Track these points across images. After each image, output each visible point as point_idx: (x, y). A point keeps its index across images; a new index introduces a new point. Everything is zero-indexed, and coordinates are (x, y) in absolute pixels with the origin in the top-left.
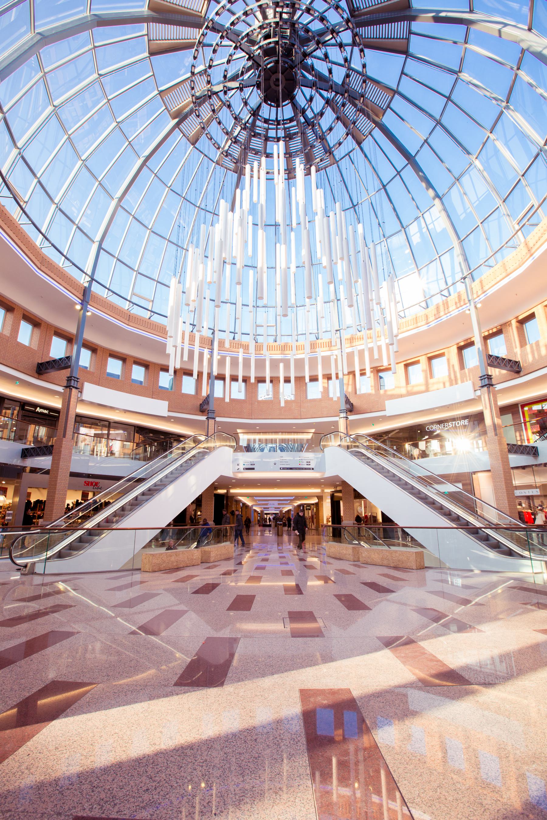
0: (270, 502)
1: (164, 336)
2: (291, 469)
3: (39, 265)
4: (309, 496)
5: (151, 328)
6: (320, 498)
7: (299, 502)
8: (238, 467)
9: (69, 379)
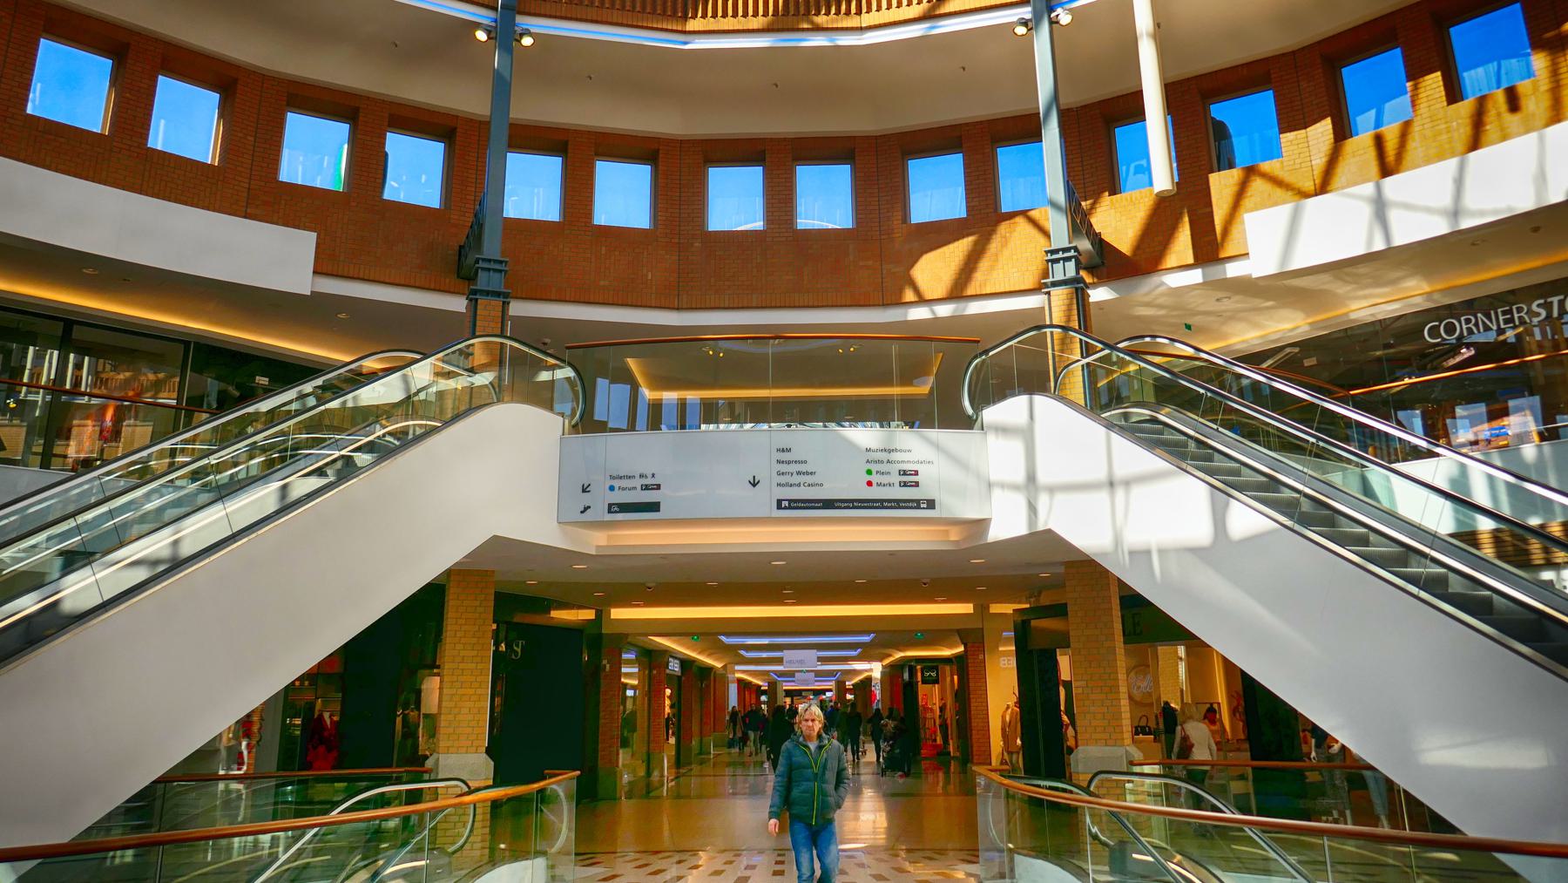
0: (787, 654)
2: (829, 504)
4: (934, 631)
6: (973, 637)
7: (899, 655)
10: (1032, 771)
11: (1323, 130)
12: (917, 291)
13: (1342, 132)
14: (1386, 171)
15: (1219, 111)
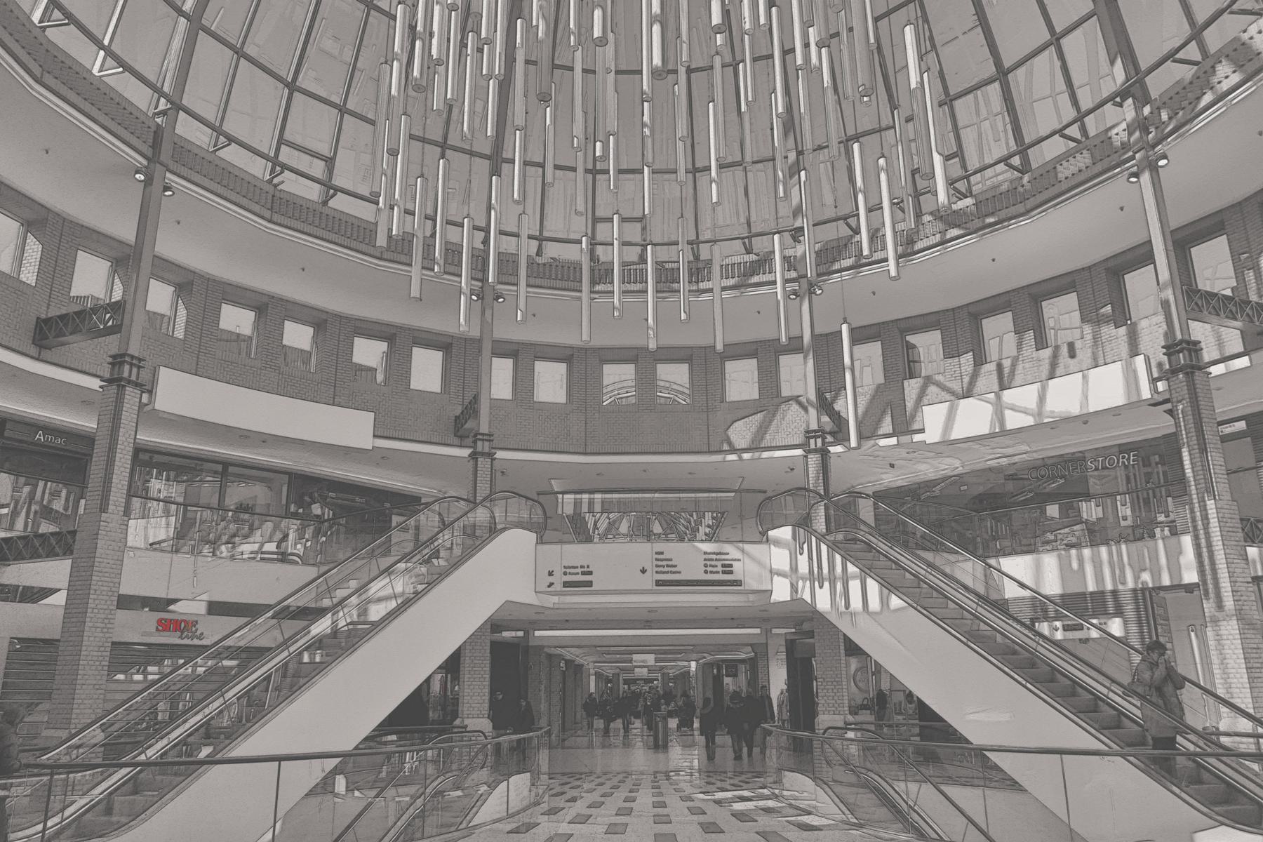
1: (511, 279)
3: (37, 71)
5: (349, 234)
8: (551, 579)
9: (118, 360)
10: (796, 727)
11: (967, 360)
12: (730, 443)
13: (980, 361)
14: (1003, 387)
15: (911, 339)
